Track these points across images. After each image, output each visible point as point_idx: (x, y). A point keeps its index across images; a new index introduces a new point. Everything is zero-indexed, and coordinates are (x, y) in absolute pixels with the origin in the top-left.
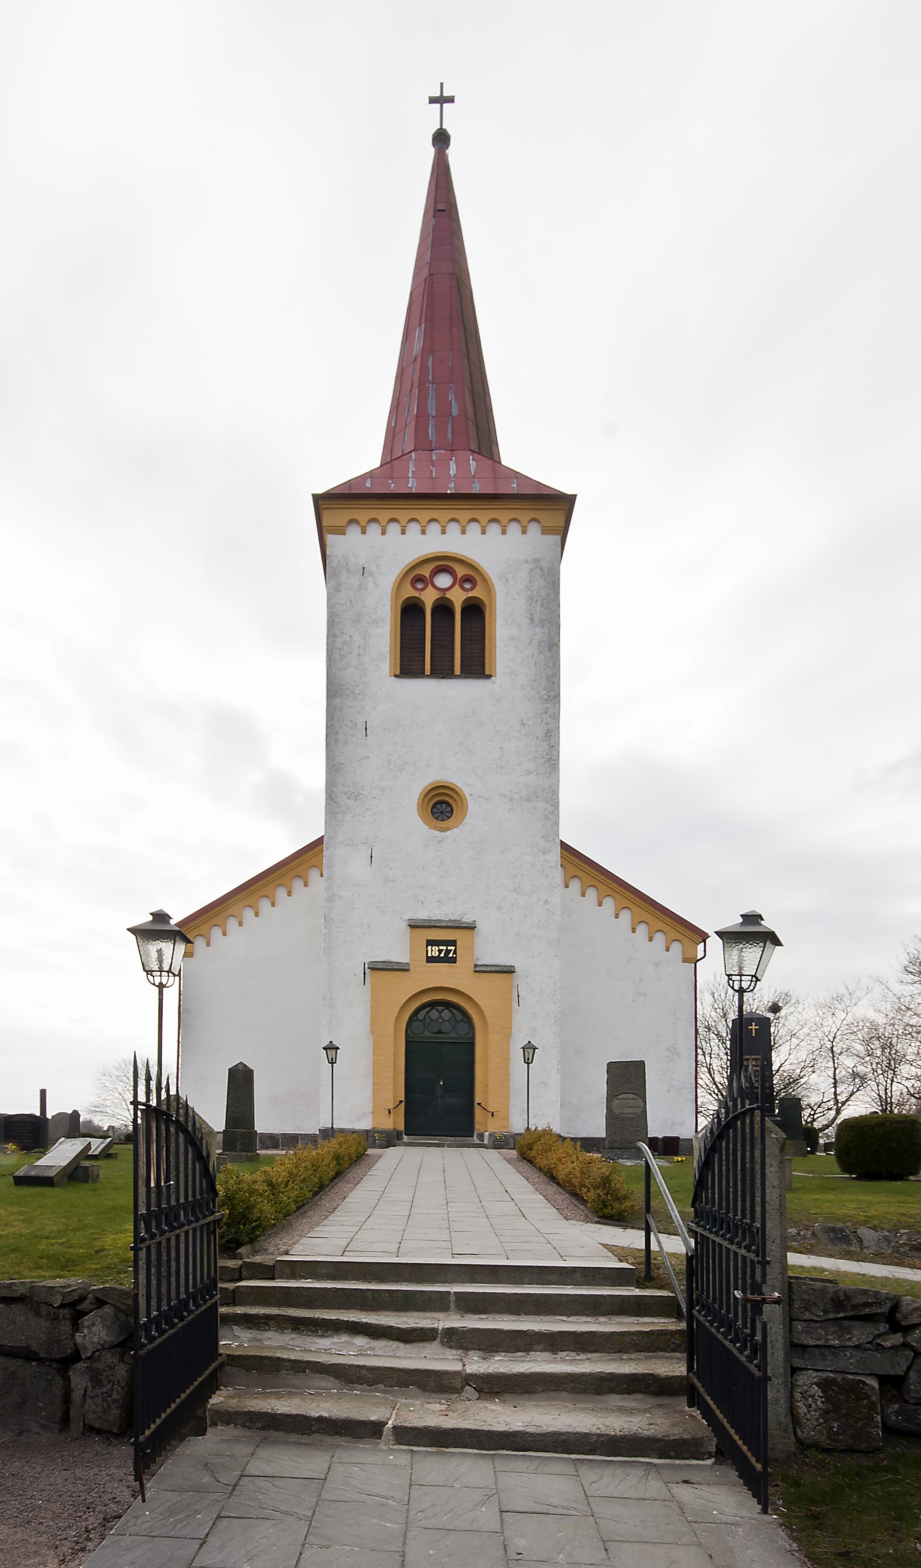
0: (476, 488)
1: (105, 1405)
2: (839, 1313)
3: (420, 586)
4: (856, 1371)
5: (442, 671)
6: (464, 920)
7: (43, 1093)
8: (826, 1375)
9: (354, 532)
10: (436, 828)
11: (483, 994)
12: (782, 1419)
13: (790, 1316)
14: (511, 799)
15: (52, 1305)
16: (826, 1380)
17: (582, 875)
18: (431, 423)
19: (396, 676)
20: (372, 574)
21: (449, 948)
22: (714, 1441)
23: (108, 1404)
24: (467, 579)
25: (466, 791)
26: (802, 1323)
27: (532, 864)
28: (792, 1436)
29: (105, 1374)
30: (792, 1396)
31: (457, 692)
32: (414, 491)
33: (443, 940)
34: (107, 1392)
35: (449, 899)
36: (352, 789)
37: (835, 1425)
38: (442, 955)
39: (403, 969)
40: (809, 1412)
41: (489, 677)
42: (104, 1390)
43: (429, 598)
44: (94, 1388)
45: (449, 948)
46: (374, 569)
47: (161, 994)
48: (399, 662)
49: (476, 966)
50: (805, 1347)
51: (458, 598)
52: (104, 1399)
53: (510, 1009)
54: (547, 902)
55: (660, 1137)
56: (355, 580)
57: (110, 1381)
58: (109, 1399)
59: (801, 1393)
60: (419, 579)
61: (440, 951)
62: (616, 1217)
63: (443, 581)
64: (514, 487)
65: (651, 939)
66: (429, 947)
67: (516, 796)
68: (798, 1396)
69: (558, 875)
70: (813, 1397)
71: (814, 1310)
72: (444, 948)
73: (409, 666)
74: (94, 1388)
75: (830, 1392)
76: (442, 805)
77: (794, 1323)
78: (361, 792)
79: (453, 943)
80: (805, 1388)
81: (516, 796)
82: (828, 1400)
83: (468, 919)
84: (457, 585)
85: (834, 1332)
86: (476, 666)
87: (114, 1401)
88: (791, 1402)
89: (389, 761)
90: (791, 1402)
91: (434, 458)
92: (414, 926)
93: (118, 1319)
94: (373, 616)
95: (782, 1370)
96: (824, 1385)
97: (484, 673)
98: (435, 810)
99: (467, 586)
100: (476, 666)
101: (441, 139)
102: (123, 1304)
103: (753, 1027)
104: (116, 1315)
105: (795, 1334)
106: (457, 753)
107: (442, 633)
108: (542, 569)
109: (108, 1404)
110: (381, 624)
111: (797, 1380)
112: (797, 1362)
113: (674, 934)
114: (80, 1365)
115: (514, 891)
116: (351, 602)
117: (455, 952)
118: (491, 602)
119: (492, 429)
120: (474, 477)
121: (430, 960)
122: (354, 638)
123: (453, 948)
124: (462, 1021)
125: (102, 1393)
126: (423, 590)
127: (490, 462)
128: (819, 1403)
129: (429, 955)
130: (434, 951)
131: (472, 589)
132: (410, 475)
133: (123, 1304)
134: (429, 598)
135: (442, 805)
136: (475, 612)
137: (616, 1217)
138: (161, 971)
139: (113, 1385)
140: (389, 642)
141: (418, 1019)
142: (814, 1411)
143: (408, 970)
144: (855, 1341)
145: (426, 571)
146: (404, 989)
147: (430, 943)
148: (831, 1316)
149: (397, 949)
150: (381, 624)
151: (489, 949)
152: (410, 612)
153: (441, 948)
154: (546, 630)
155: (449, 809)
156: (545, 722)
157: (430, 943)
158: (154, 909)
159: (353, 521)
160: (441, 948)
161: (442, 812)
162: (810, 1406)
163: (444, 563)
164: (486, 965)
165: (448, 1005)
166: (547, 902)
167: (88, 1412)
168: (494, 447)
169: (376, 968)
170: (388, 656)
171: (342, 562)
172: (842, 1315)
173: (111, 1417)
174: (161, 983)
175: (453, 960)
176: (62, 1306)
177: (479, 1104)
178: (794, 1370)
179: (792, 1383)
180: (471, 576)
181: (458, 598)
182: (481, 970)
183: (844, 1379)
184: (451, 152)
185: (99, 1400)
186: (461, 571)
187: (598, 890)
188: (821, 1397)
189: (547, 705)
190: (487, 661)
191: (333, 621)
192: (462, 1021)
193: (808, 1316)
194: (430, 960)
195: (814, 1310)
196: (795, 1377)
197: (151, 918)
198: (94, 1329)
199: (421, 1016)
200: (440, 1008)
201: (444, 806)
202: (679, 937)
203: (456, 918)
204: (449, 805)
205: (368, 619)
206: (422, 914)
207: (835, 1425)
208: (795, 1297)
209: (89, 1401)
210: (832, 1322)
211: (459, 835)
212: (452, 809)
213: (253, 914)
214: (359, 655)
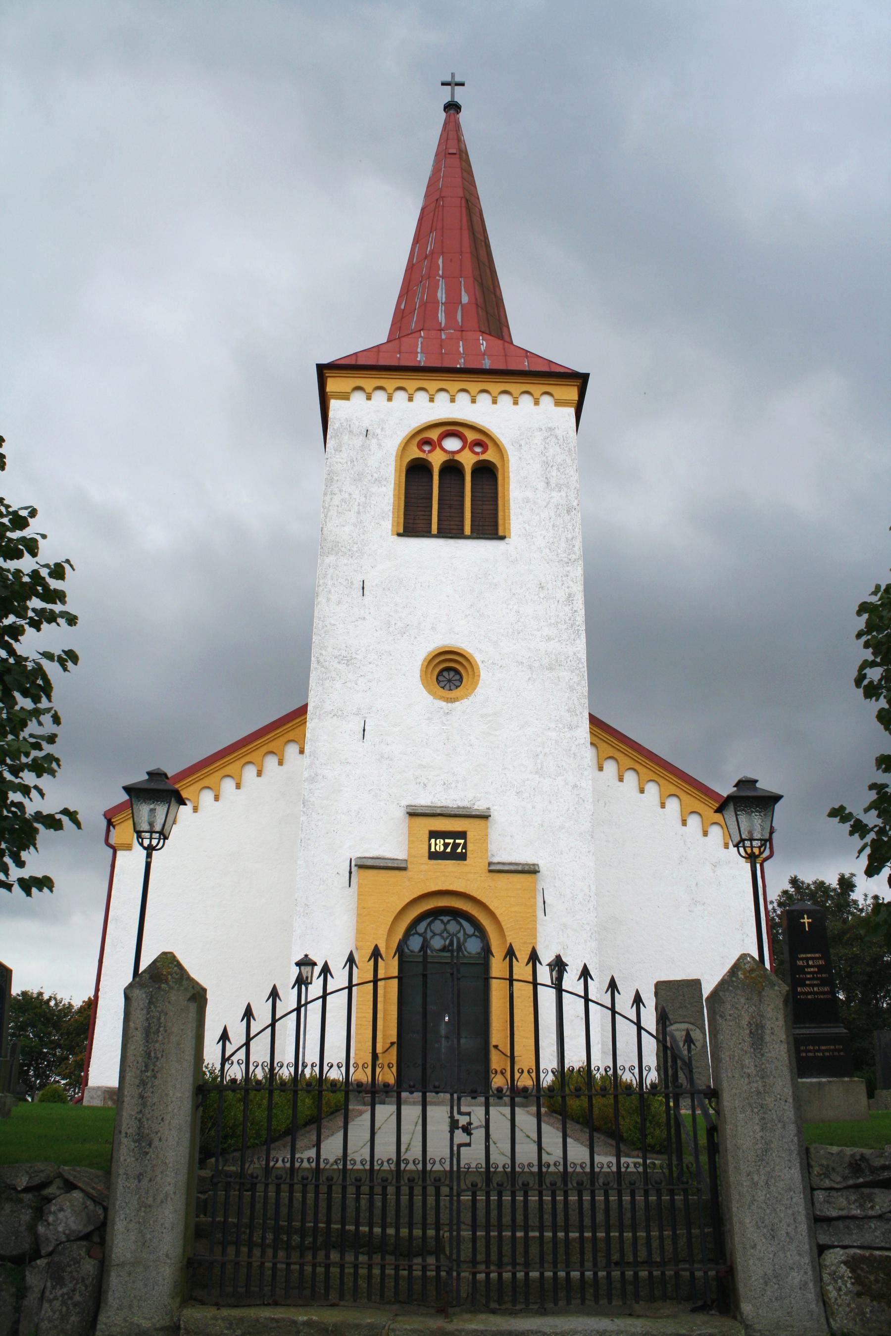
0: (487, 364)
1: (64, 1309)
2: (858, 1178)
3: (427, 448)
4: (883, 1244)
5: (451, 530)
6: (476, 807)
8: (852, 1251)
9: (358, 398)
10: (442, 698)
11: (498, 896)
12: (813, 1306)
13: (810, 1184)
14: (530, 667)
15: (15, 1189)
16: (853, 1257)
17: (617, 755)
18: (441, 308)
19: (399, 535)
20: (375, 435)
21: (457, 841)
23: (68, 1309)
26: (823, 1192)
27: (556, 742)
28: (826, 1327)
29: (69, 1269)
30: (821, 1280)
32: (422, 364)
33: (450, 833)
34: (67, 1294)
35: (458, 782)
36: (344, 653)
37: (868, 1310)
38: (449, 850)
39: (398, 867)
40: (840, 1296)
41: (503, 538)
42: (65, 1290)
43: (437, 459)
44: (53, 1288)
45: (457, 841)
46: (378, 431)
47: (149, 856)
48: (402, 521)
49: (490, 864)
50: (828, 1220)
51: (468, 460)
52: (63, 1303)
53: (534, 919)
54: (576, 786)
56: (358, 441)
57: (73, 1278)
58: (70, 1302)
59: (829, 1274)
60: (427, 442)
61: (446, 845)
62: (658, 1148)
63: (453, 444)
64: (525, 365)
65: (705, 834)
66: (433, 841)
67: (536, 664)
68: (826, 1277)
69: (588, 754)
70: (842, 1277)
71: (834, 1176)
72: (451, 841)
73: (413, 525)
74: (53, 1288)
75: (859, 1271)
76: (450, 671)
77: (816, 1193)
78: (354, 656)
79: (463, 835)
80: (833, 1268)
81: (536, 664)
82: (858, 1280)
83: (480, 806)
84: (467, 449)
85: (856, 1201)
86: (489, 526)
87: (75, 1305)
88: (821, 1287)
89: (389, 623)
90: (821, 1287)
91: (443, 337)
92: (414, 814)
93: (86, 1207)
94: (376, 476)
95: (807, 1247)
96: (852, 1263)
97: (497, 533)
98: (441, 678)
99: (478, 449)
100: (489, 526)
101: (453, 107)
102: (94, 1188)
103: (806, 920)
104: (84, 1203)
105: (817, 1205)
106: (466, 616)
108: (556, 437)
109: (68, 1309)
110: (384, 483)
111: (824, 1260)
112: (823, 1239)
113: (626, 762)
114: (42, 1262)
115: (536, 773)
116: (352, 461)
117: (465, 846)
118: (503, 465)
119: (502, 314)
120: (484, 354)
121: (434, 856)
122: (354, 496)
123: (462, 841)
124: (474, 935)
125: (62, 1295)
126: (430, 452)
127: (500, 342)
128: (849, 1285)
129: (433, 849)
130: (438, 845)
131: (483, 452)
132: (419, 350)
133: (94, 1188)
134: (437, 459)
135: (450, 671)
136: (488, 475)
137: (658, 1148)
138: (151, 832)
139: (76, 1284)
140: (392, 501)
141: (417, 933)
142: (846, 1294)
143: (404, 869)
144: (878, 1210)
145: (434, 435)
146: (402, 891)
147: (434, 835)
148: (851, 1182)
149: (391, 841)
150: (384, 483)
151: (506, 842)
152: (416, 472)
153: (447, 841)
154: (563, 494)
155: (457, 677)
156: (566, 585)
157: (434, 835)
158: (151, 768)
159: (359, 388)
160: (447, 841)
161: (449, 681)
162: (840, 1289)
163: (452, 429)
164: (503, 864)
165: (456, 914)
166: (576, 786)
167: (42, 1320)
168: (505, 329)
169: (364, 866)
170: (391, 514)
171: (345, 424)
172: (861, 1180)
173: (69, 1327)
174: (150, 845)
175: (463, 857)
176: (27, 1190)
177: (496, 1047)
178: (822, 1249)
179: (820, 1265)
180: (483, 439)
181: (468, 460)
182: (496, 870)
183: (871, 1255)
185: (57, 1304)
186: (471, 436)
187: (638, 773)
188: (851, 1278)
189: (569, 568)
190: (500, 522)
191: (332, 479)
192: (474, 935)
193: (827, 1183)
194: (434, 856)
195: (834, 1176)
196: (824, 1256)
197: (147, 777)
198: (61, 1215)
199: (421, 927)
200: (446, 919)
201: (452, 674)
202: (655, 777)
203: (465, 804)
204: (457, 672)
205: (370, 478)
206: (424, 800)
207: (868, 1310)
208: (813, 1163)
209: (46, 1305)
210: (853, 1190)
211: (467, 707)
212: (461, 678)
213: (255, 773)
214: (359, 513)
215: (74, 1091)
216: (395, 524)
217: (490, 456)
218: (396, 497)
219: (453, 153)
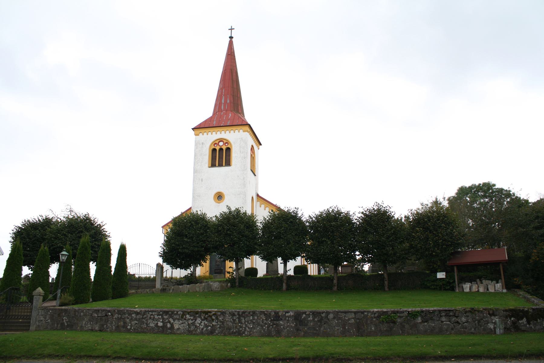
5: (220, 165)
7: (255, 175)
22: (35, 293)
24: (226, 143)
25: (225, 193)
31: (224, 170)
43: (218, 148)
51: (224, 148)
55: (402, 208)
63: (221, 144)
86: (228, 164)
100: (228, 164)
101: (231, 38)
107: (221, 156)
134: (218, 148)
136: (228, 150)
145: (217, 142)
152: (214, 150)
163: (221, 140)
180: (227, 142)
181: (224, 148)
184: (233, 39)
186: (225, 141)
215: (264, 330)
216: (209, 164)
217: (229, 146)
218: (209, 158)
219: (231, 44)
